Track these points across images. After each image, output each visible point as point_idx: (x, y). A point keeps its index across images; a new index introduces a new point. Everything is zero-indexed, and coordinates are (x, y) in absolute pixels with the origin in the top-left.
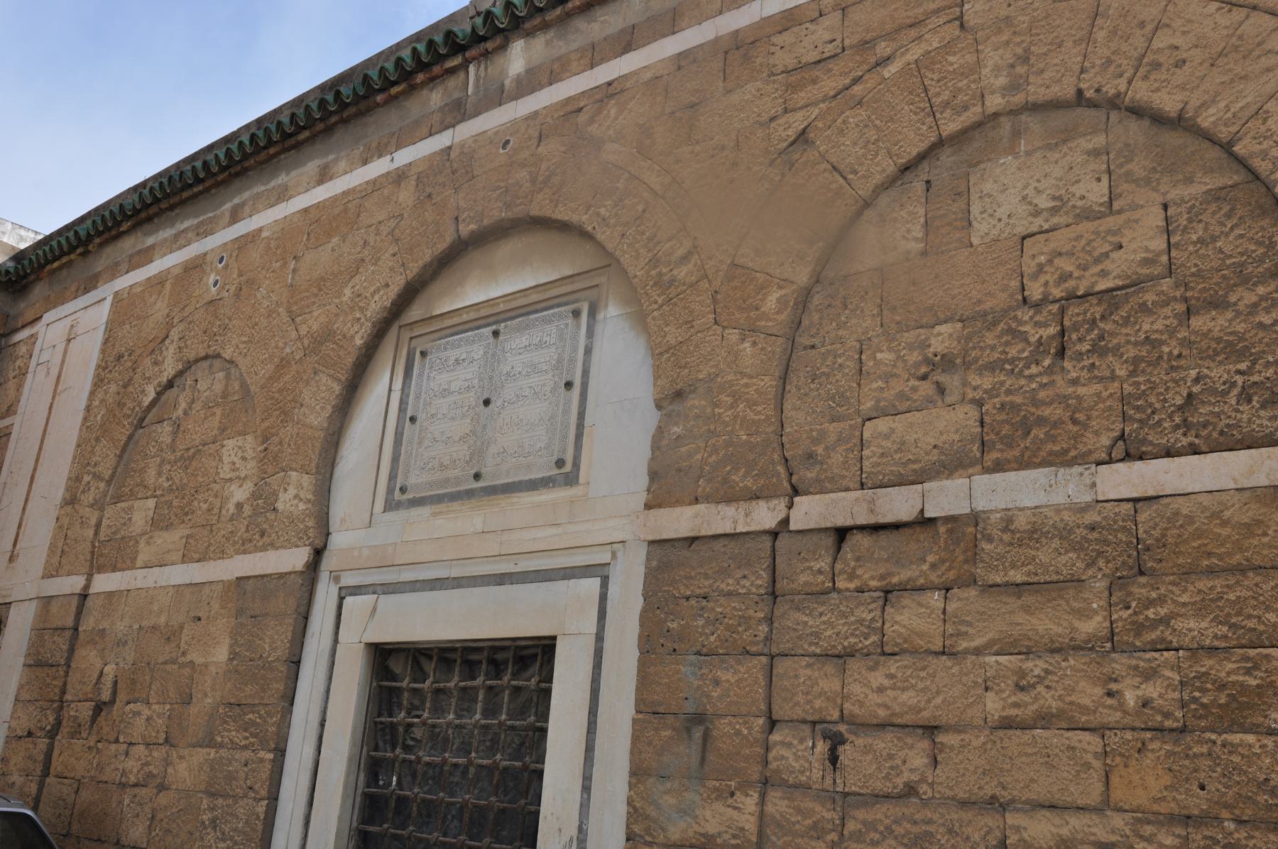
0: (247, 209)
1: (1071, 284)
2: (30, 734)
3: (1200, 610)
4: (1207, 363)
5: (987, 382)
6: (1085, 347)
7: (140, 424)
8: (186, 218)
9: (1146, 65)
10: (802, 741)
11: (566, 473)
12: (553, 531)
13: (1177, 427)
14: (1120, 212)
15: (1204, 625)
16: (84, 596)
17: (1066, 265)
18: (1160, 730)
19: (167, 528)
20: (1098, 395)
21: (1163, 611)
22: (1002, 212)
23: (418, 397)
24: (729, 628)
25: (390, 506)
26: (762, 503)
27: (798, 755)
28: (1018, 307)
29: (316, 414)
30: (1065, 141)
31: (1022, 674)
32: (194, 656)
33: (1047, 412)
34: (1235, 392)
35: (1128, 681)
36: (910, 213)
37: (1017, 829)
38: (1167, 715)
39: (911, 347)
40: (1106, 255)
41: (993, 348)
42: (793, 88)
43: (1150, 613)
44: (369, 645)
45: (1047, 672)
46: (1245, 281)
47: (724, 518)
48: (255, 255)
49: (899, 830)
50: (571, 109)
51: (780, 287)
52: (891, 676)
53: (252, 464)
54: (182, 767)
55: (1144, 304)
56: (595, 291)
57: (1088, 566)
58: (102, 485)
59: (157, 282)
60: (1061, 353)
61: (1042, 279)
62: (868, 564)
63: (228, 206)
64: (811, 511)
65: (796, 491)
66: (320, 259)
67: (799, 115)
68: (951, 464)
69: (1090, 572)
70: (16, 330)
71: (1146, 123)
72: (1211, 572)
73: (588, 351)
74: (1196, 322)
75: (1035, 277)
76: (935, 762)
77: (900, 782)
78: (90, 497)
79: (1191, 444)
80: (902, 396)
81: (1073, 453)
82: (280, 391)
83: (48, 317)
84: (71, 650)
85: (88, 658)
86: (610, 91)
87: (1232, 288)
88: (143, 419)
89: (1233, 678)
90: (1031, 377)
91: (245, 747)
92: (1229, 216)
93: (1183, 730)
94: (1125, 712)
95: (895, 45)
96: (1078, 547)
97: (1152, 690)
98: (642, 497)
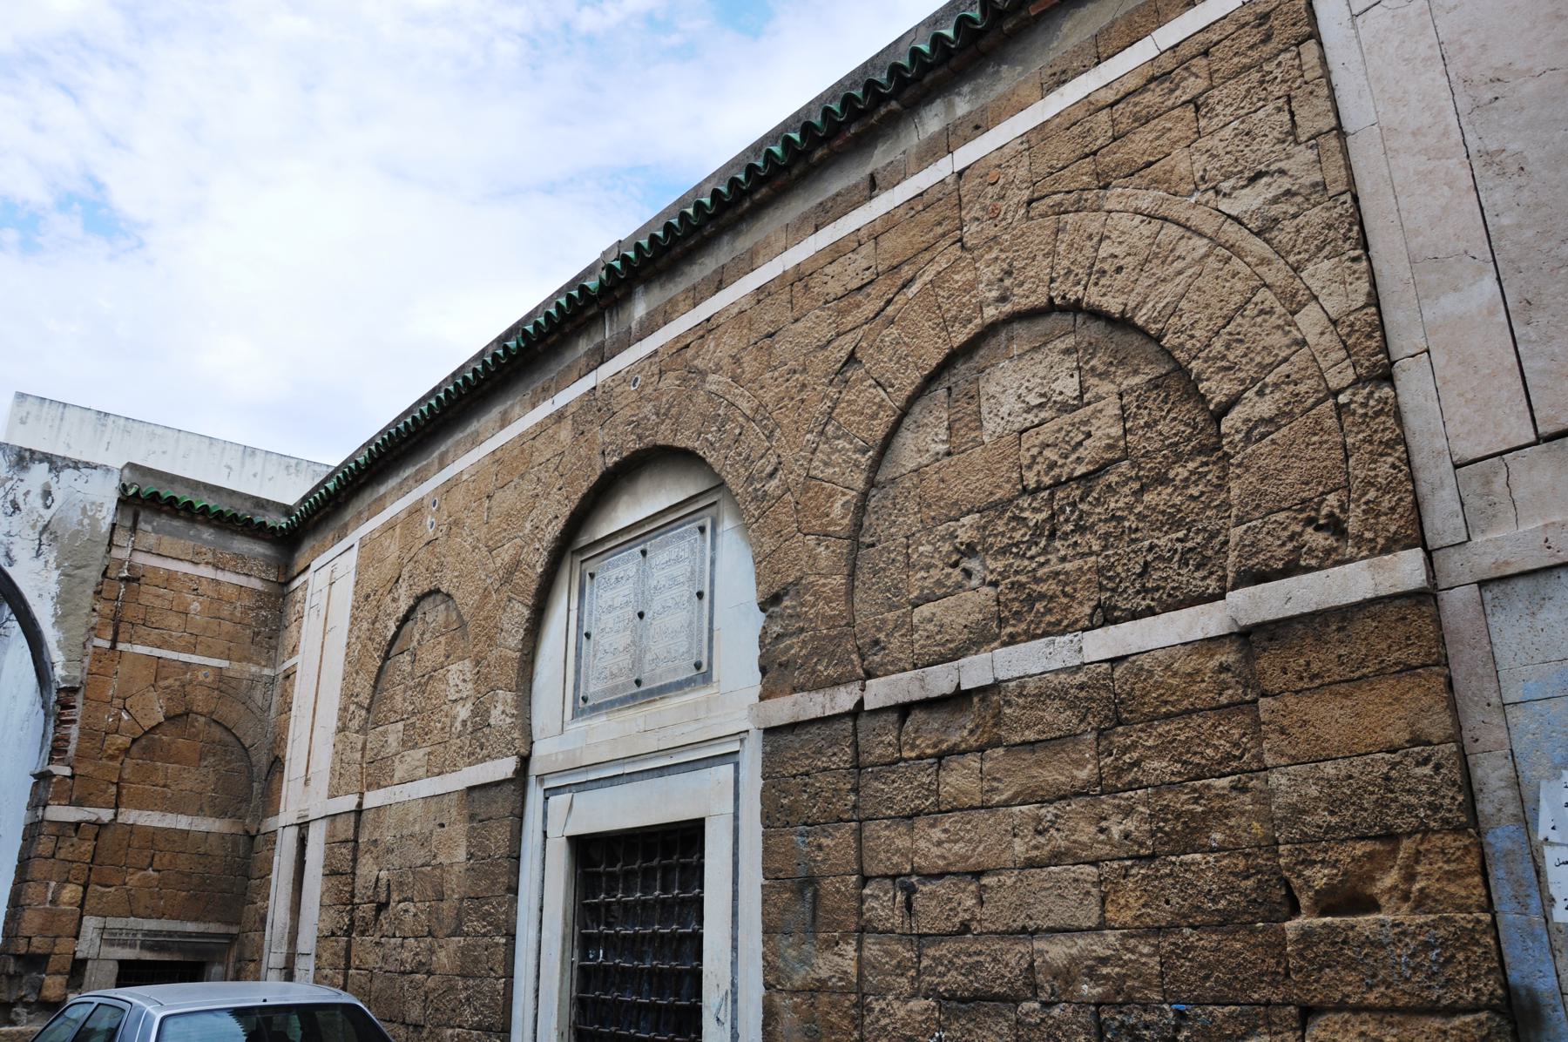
0: (451, 455)
1: (1057, 471)
2: (333, 934)
3: (1159, 751)
4: (1156, 534)
5: (999, 565)
6: (1070, 527)
7: (386, 658)
8: (407, 466)
9: (1096, 273)
10: (886, 893)
11: (702, 674)
12: (694, 726)
13: (1138, 593)
14: (1089, 404)
15: (1164, 764)
16: (359, 811)
17: (1051, 454)
18: (1139, 858)
19: (413, 748)
20: (1080, 569)
21: (1135, 755)
22: (1004, 410)
23: (590, 614)
24: (828, 801)
25: (577, 714)
26: (842, 688)
27: (882, 904)
28: (1020, 495)
29: (513, 639)
30: (1045, 344)
31: (1039, 820)
32: (441, 859)
33: (1043, 588)
34: (1176, 558)
35: (1114, 818)
36: (937, 418)
37: (1041, 953)
38: (1141, 845)
39: (943, 538)
40: (1080, 444)
41: (1003, 534)
42: (842, 313)
43: (1126, 758)
44: (569, 838)
45: (1056, 816)
46: (1179, 458)
47: (814, 705)
48: (458, 497)
49: (958, 962)
50: (681, 346)
51: (844, 494)
52: (945, 831)
53: (470, 686)
54: (442, 954)
55: (1109, 486)
56: (713, 509)
57: (1081, 721)
58: (363, 713)
59: (390, 526)
60: (1052, 535)
61: (1036, 468)
62: (928, 733)
63: (436, 454)
64: (880, 692)
65: (869, 675)
66: (507, 499)
67: (849, 337)
68: (979, 639)
69: (1082, 727)
70: (294, 578)
71: (1102, 324)
72: (1168, 716)
73: (713, 562)
74: (1147, 498)
75: (1030, 467)
76: (982, 903)
77: (957, 920)
78: (355, 724)
79: (1149, 607)
80: (939, 583)
81: (1065, 623)
82: (485, 619)
83: (315, 565)
84: (355, 860)
85: (367, 869)
86: (708, 328)
87: (1170, 467)
88: (388, 652)
89: (1186, 807)
90: (1032, 558)
91: (484, 935)
92: (1165, 401)
93: (1152, 857)
94: (1113, 845)
95: (914, 268)
96: (1072, 706)
97: (1130, 825)
98: (758, 689)
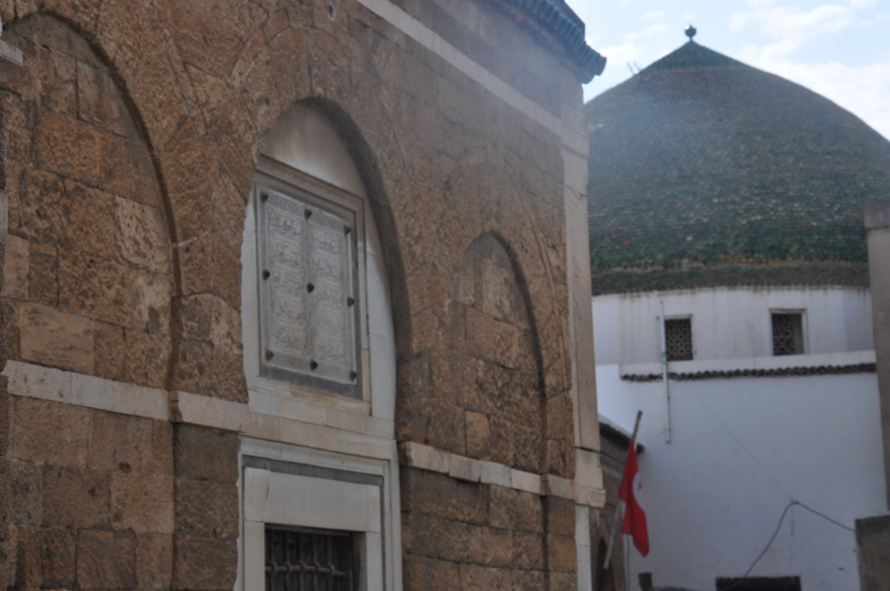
19: (57, 303)
44: (267, 524)
